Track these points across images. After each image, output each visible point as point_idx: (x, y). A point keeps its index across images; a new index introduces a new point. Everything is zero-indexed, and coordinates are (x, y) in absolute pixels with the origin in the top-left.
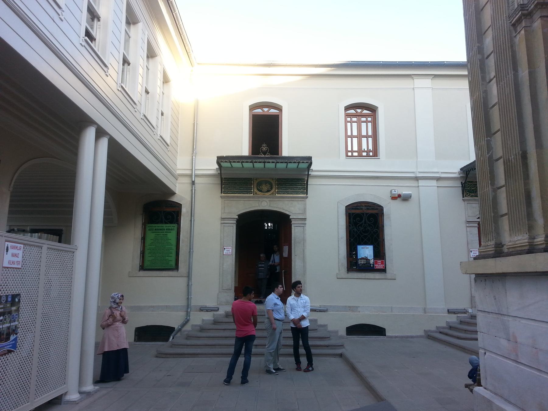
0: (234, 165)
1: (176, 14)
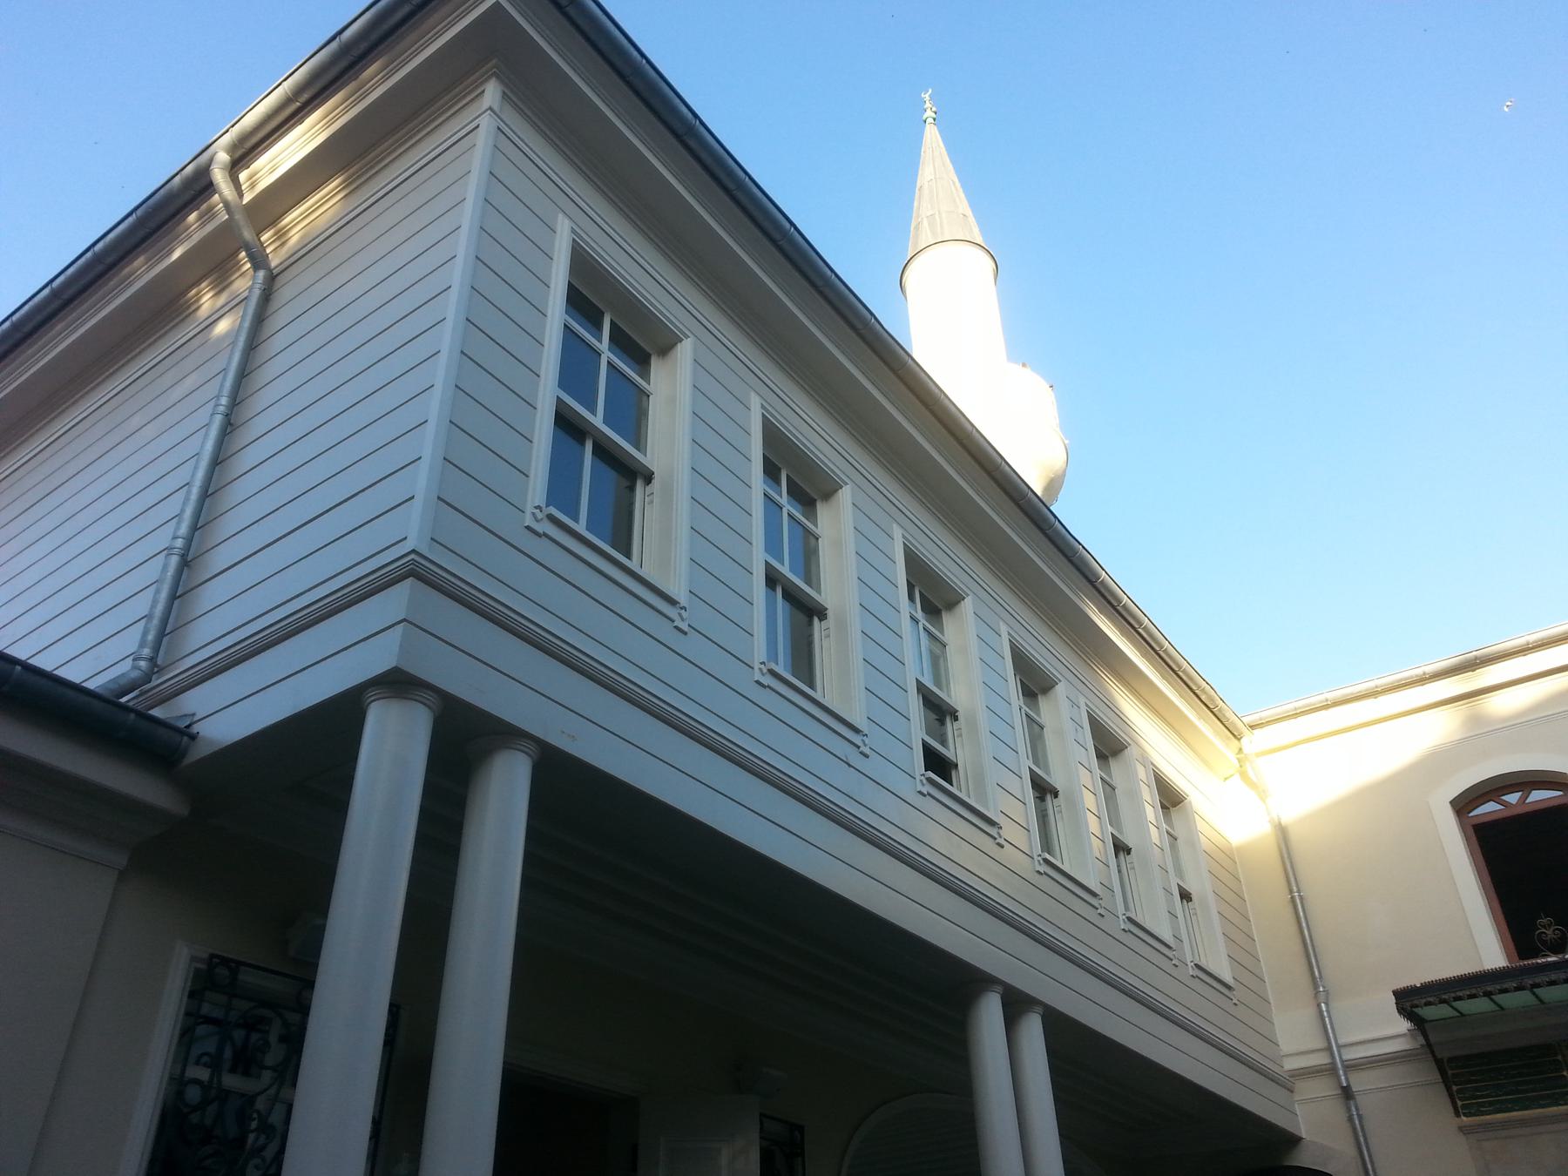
0: (1466, 1006)
1: (1145, 629)
